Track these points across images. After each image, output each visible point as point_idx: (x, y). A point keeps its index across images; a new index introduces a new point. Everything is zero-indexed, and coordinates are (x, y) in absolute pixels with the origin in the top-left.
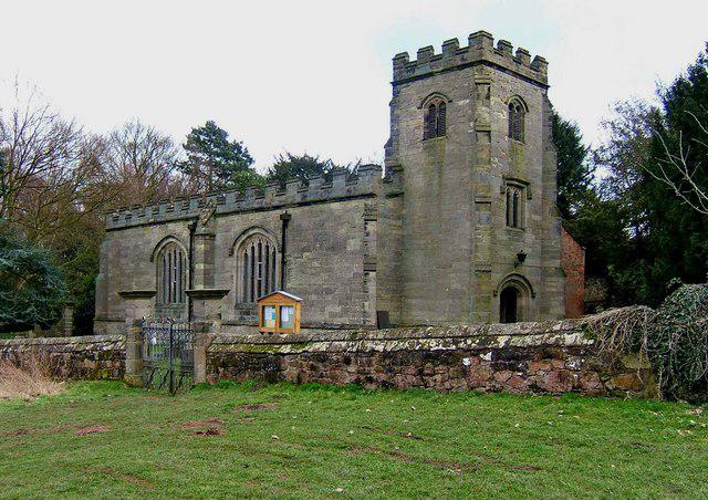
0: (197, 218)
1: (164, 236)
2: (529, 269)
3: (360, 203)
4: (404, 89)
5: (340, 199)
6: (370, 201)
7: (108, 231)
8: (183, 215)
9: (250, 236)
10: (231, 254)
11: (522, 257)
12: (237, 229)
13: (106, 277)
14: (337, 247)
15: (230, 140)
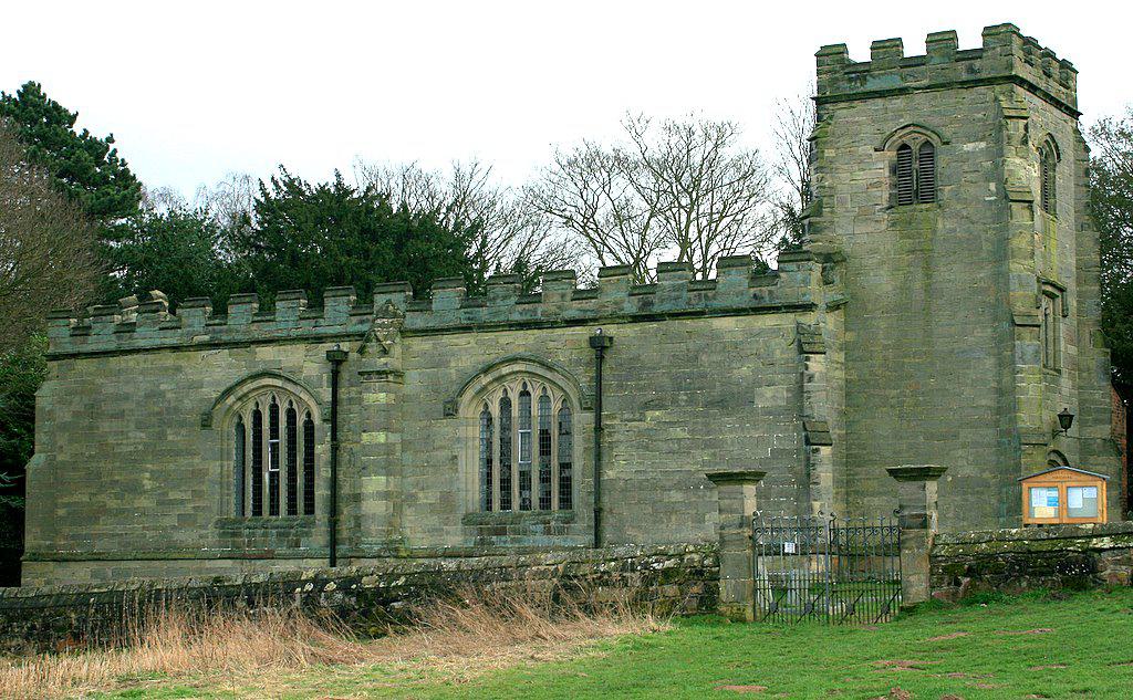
1: (245, 373)
3: (787, 321)
4: (842, 112)
5: (738, 312)
7: (55, 357)
8: (307, 328)
9: (500, 379)
13: (51, 461)
14: (733, 401)
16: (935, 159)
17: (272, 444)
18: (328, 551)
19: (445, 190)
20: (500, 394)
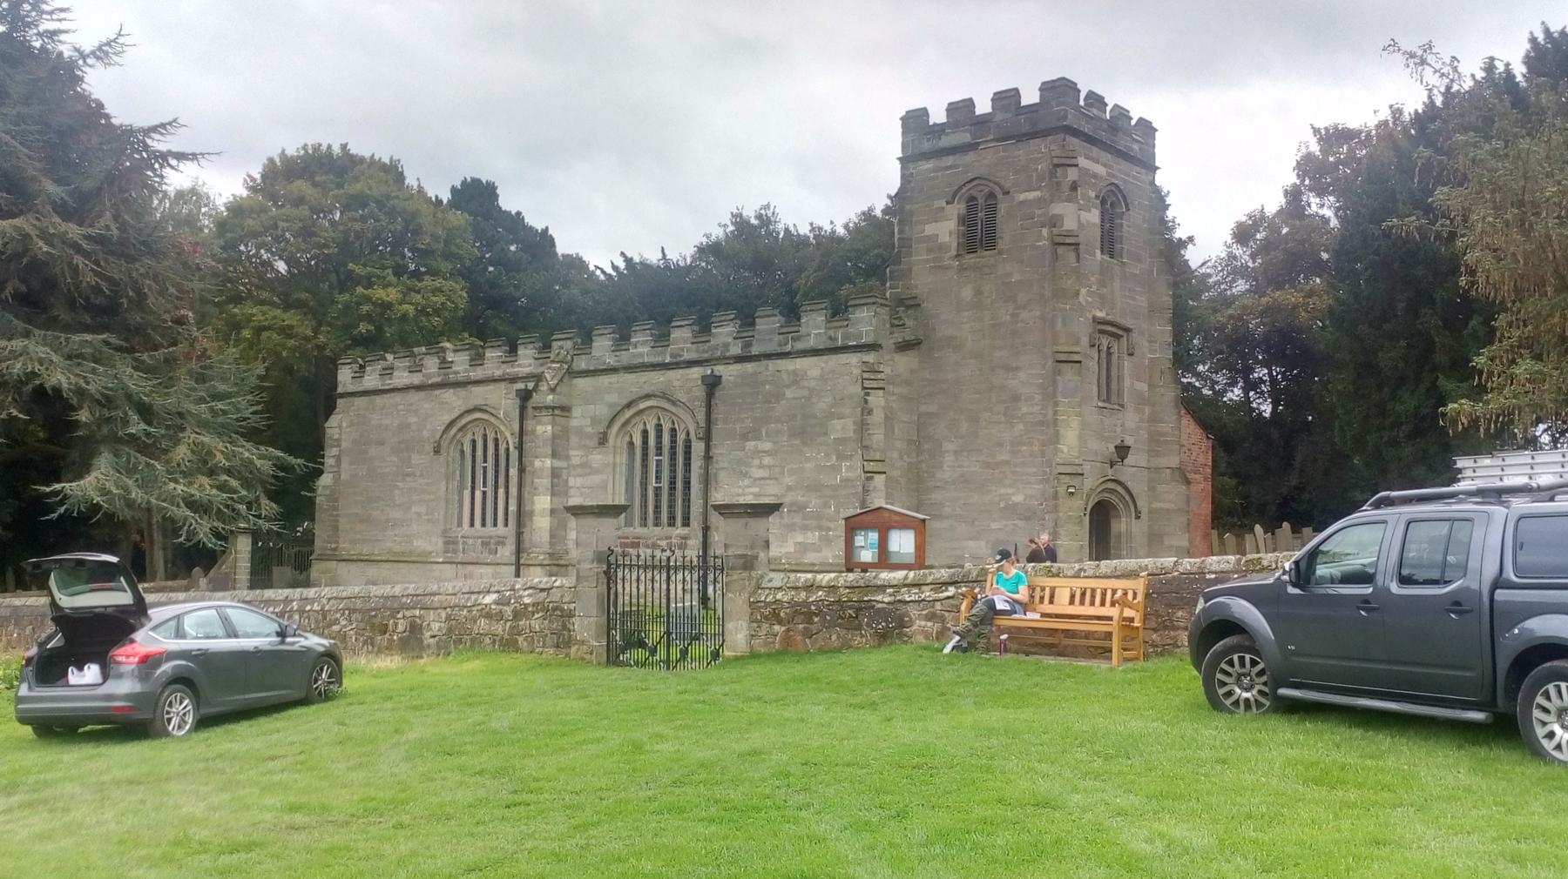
0: (538, 378)
2: (1132, 473)
5: (815, 352)
6: (870, 357)
9: (640, 412)
10: (603, 440)
11: (1122, 451)
12: (615, 398)
15: (1170, 214)
16: (999, 206)
17: (661, 455)
18: (513, 558)
19: (231, 199)
20: (641, 427)
